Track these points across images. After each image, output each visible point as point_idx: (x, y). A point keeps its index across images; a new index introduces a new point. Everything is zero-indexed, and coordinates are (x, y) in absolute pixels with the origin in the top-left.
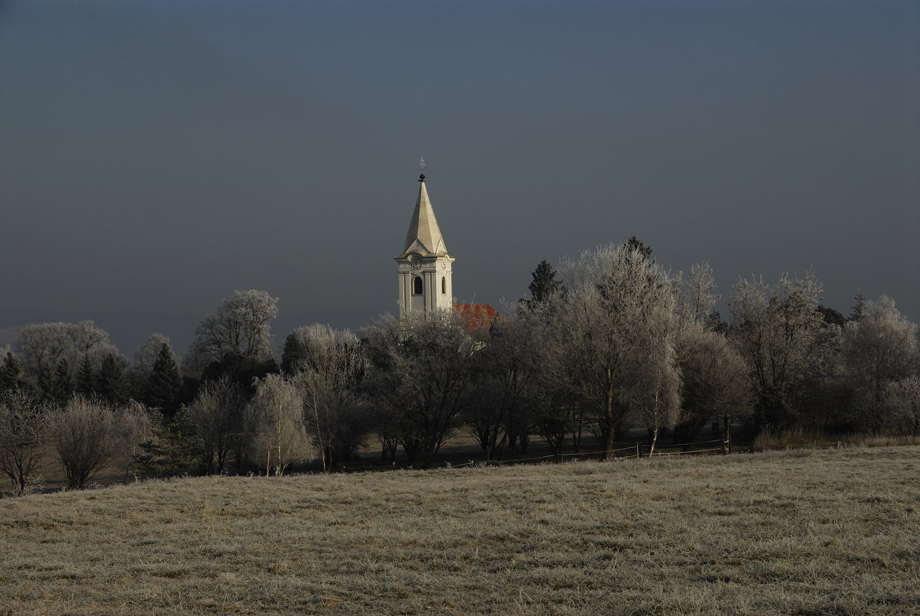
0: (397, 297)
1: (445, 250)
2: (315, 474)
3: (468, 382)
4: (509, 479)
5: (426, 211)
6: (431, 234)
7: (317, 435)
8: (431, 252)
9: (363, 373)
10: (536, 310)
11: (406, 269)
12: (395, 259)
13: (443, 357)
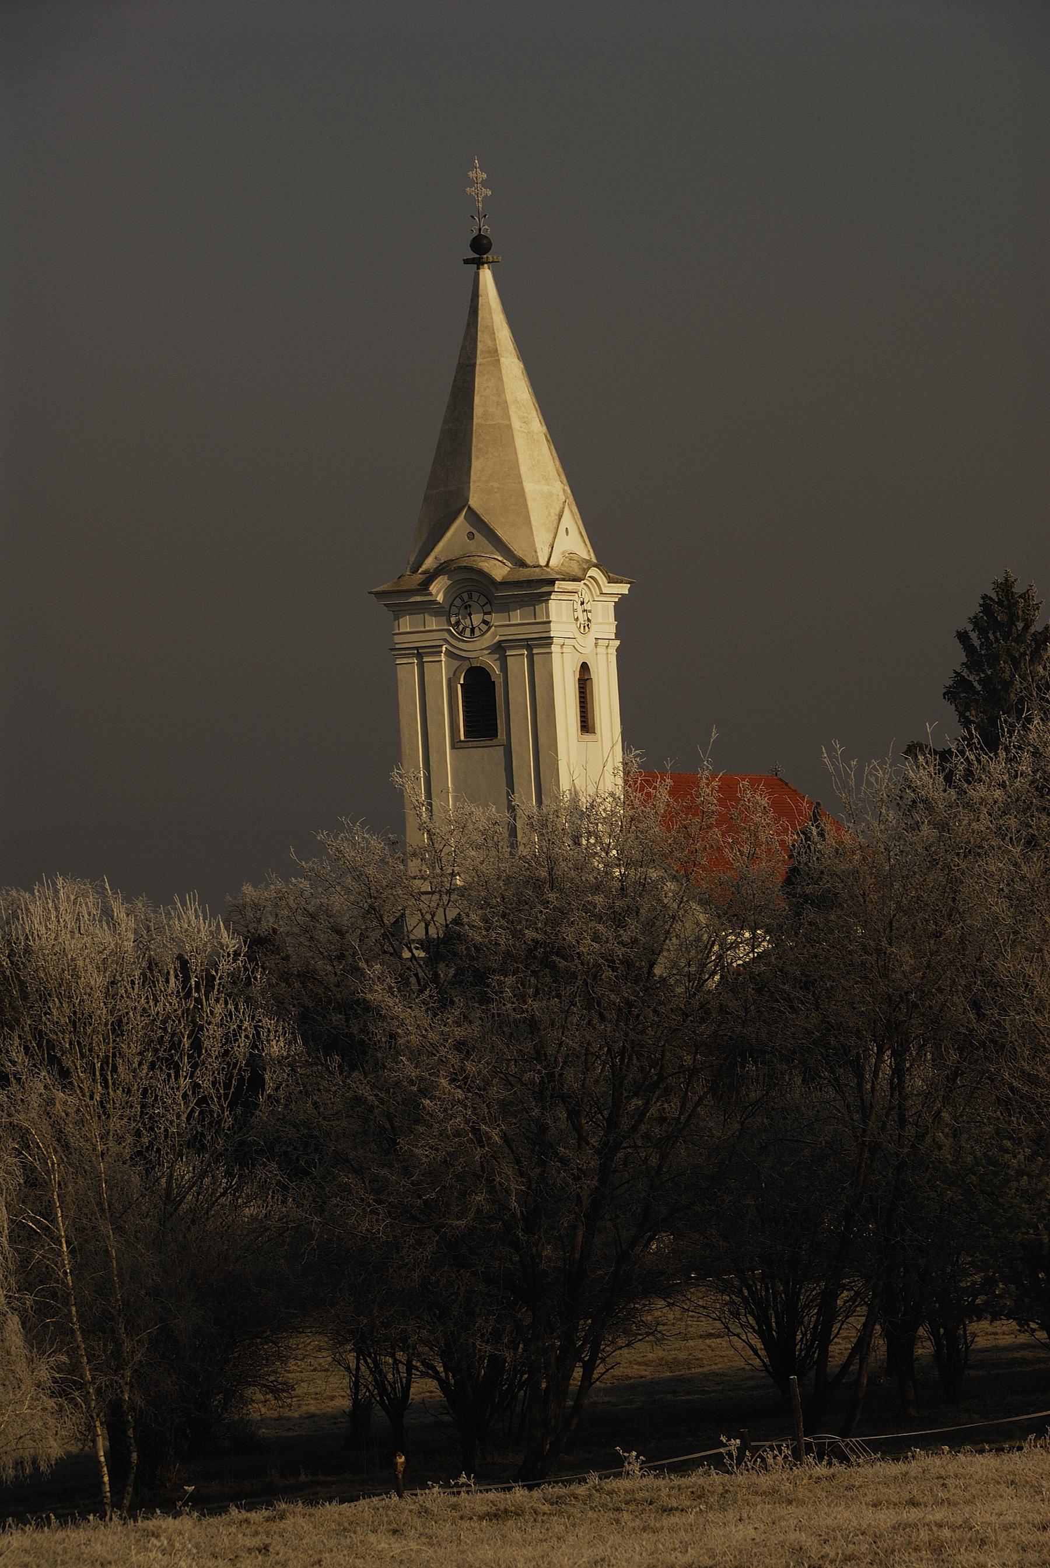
0: (394, 754)
1: (584, 551)
2: (63, 1524)
3: (698, 1103)
4: (886, 1518)
5: (500, 390)
6: (529, 487)
7: (72, 1353)
8: (529, 562)
9: (257, 1082)
10: (978, 792)
11: (424, 636)
12: (376, 594)
13: (591, 1002)
